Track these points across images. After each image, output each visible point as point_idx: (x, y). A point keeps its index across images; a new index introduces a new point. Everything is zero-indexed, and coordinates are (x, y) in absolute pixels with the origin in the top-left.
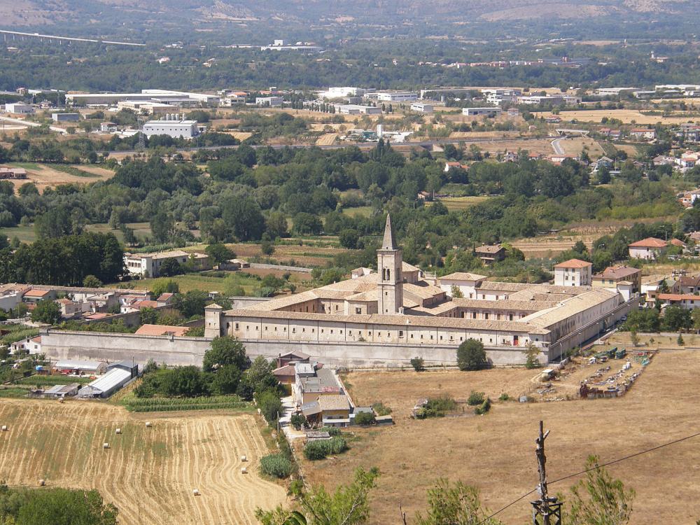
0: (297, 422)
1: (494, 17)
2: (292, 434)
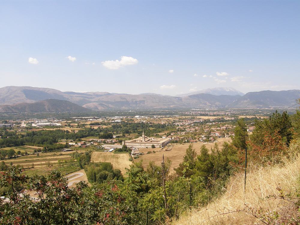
0: (133, 154)
1: (155, 108)
2: (132, 156)
